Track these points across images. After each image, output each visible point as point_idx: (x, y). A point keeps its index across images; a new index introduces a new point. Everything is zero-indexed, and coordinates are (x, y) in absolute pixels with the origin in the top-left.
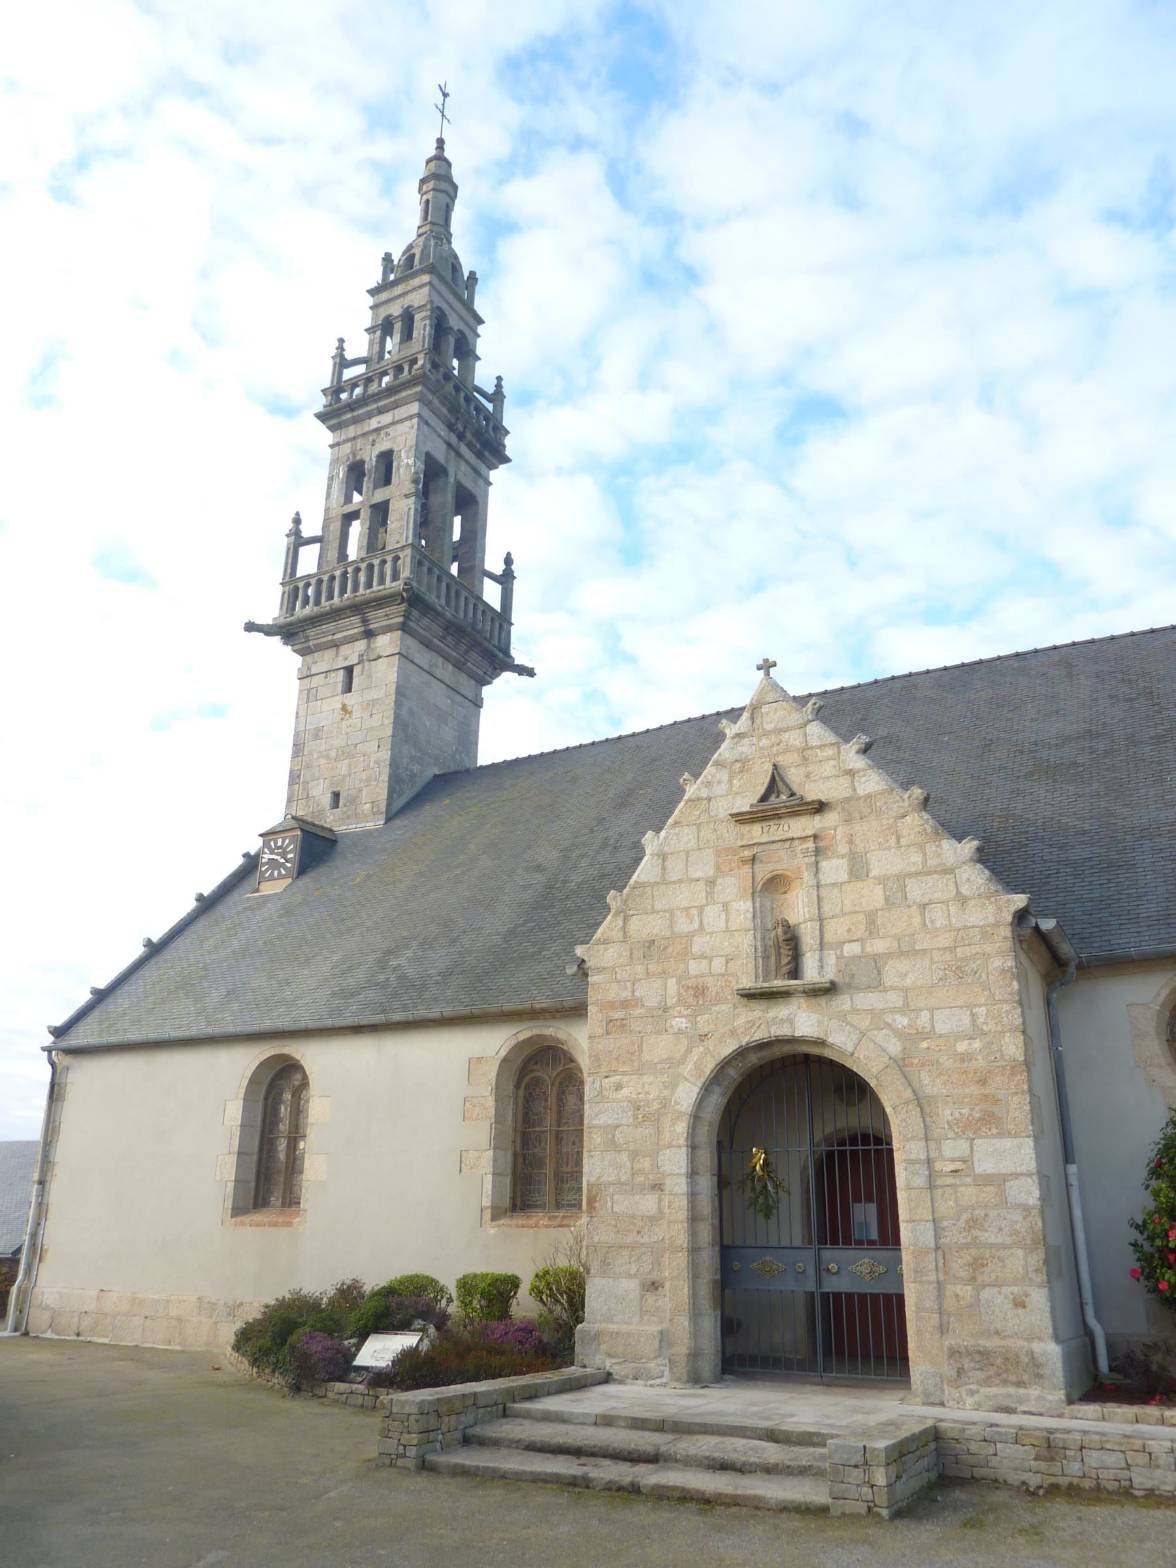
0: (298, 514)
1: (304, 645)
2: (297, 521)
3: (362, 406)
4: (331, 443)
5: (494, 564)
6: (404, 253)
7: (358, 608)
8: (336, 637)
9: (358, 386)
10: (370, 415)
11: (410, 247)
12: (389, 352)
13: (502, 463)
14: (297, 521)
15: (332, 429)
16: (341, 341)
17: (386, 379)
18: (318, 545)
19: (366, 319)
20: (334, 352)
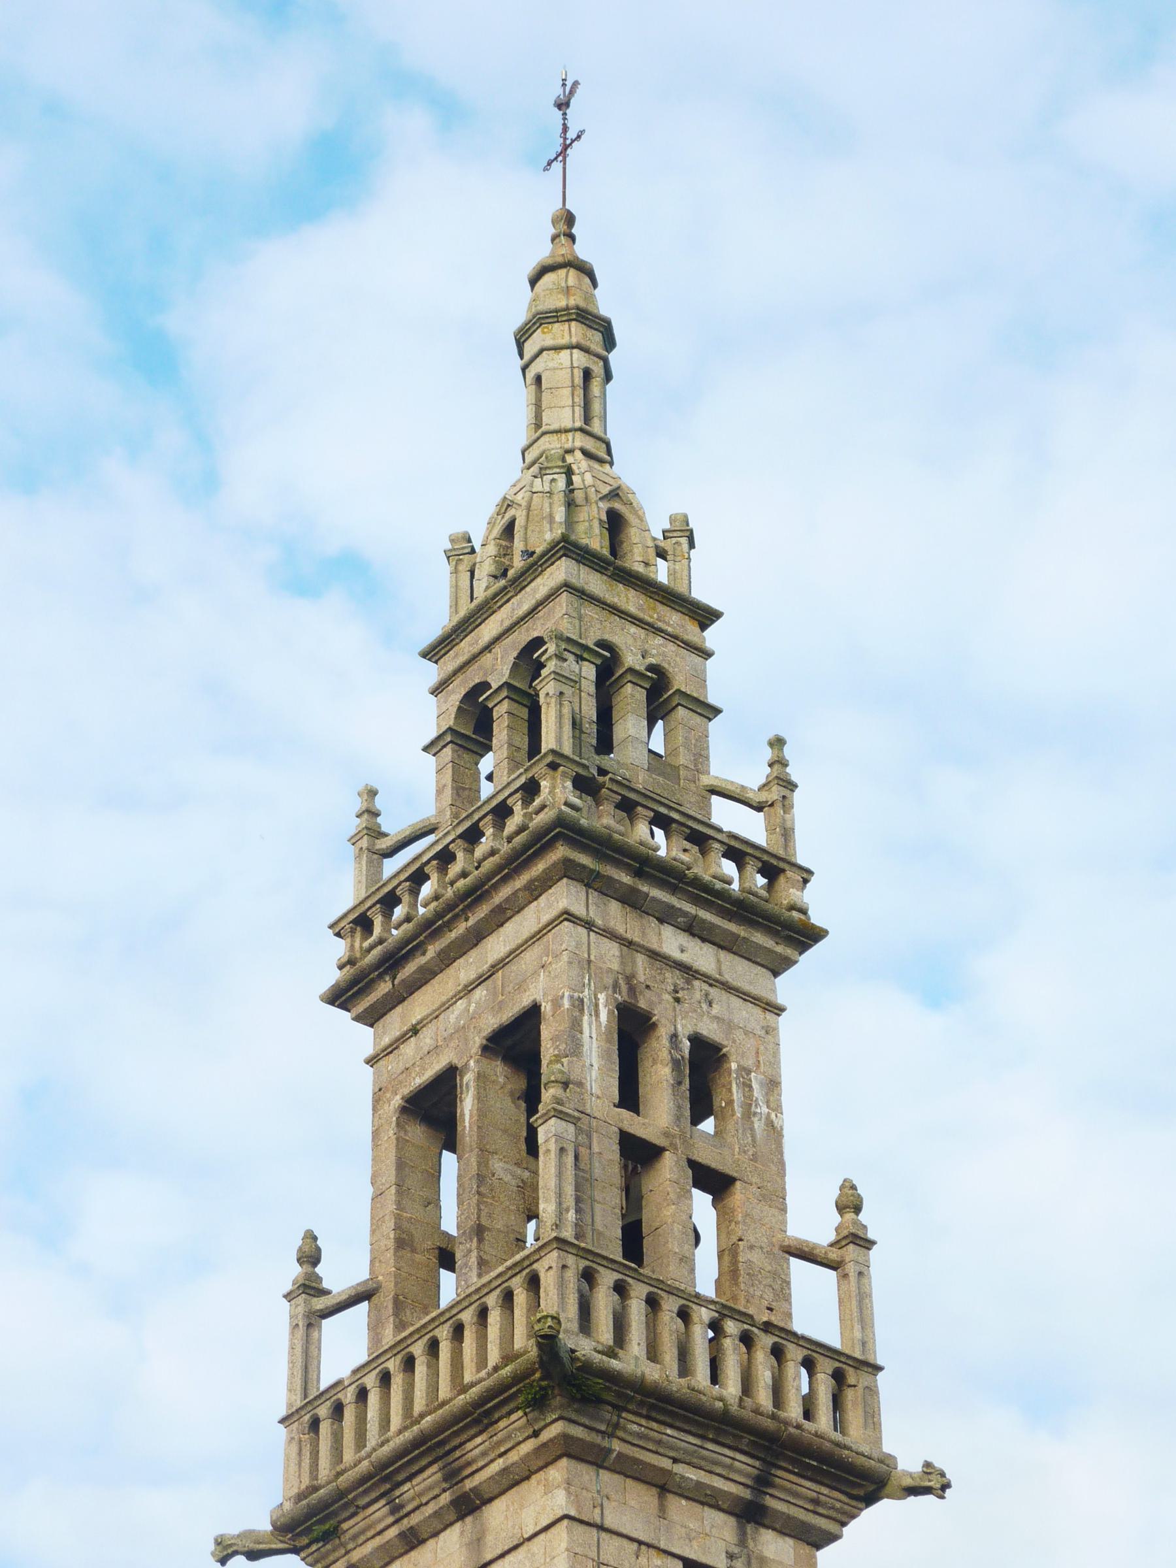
0: (311, 1237)
1: (597, 1439)
2: (310, 1256)
3: (662, 884)
4: (369, 1051)
5: (811, 1218)
6: (491, 523)
7: (435, 1446)
8: (679, 1469)
9: (427, 878)
10: (666, 916)
11: (506, 504)
12: (490, 778)
13: (803, 947)
14: (310, 1256)
15: (370, 1018)
16: (778, 743)
17: (427, 889)
18: (365, 1305)
19: (428, 716)
20: (354, 825)
